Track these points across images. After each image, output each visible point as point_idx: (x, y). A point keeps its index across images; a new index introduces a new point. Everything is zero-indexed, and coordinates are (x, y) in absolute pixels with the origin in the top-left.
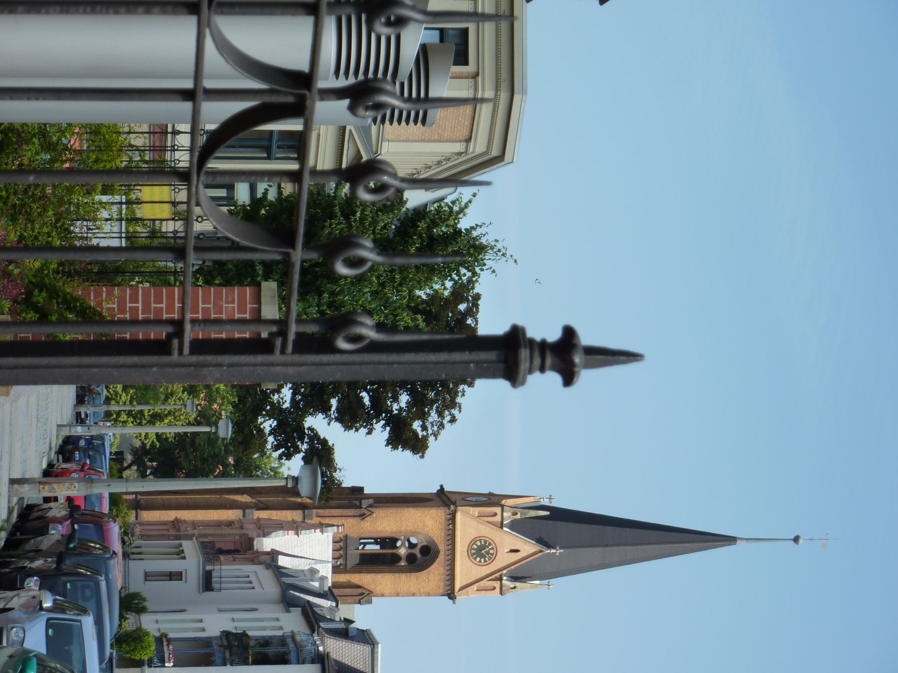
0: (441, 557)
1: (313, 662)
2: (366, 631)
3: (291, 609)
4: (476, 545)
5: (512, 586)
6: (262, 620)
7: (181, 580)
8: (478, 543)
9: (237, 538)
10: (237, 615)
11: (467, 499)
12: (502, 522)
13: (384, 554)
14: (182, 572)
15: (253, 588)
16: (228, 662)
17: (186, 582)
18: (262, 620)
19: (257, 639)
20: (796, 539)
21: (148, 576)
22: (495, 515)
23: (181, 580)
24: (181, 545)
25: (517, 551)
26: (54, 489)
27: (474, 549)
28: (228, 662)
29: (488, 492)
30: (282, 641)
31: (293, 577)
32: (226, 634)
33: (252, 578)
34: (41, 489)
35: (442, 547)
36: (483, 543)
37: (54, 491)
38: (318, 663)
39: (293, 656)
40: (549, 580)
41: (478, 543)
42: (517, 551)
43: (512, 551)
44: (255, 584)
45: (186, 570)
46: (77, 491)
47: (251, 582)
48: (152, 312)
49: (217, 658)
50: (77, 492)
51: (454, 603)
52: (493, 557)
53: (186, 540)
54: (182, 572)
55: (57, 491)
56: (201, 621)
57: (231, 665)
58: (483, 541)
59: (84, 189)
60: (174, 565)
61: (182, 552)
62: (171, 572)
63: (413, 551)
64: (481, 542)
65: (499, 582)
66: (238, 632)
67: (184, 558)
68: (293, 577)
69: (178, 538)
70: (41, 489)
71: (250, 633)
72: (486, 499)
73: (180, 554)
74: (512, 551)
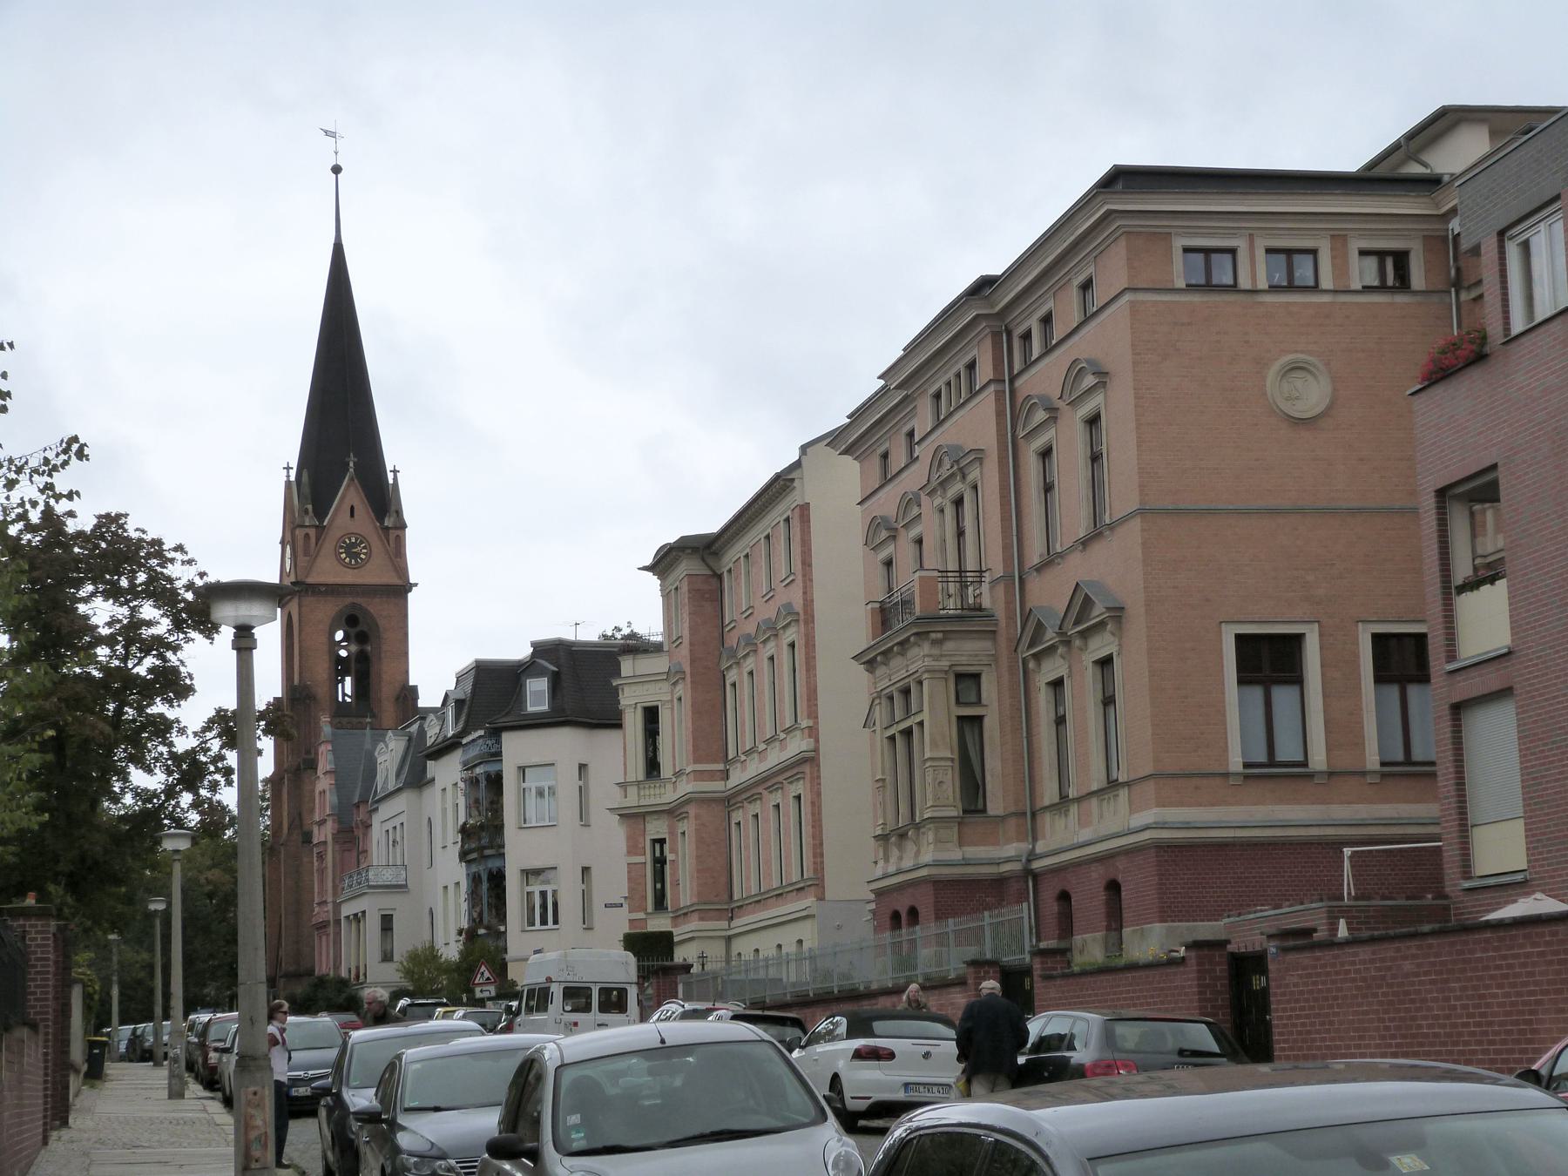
0: (359, 600)
1: (499, 742)
2: (457, 678)
3: (429, 776)
4: (345, 558)
5: (395, 515)
6: (444, 810)
7: (392, 915)
8: (343, 556)
9: (337, 847)
10: (438, 843)
11: (288, 570)
12: (317, 527)
13: (357, 672)
14: (382, 916)
15: (402, 824)
16: (502, 851)
17: (1494, 467)
18: (444, 810)
19: (469, 815)
20: (337, 170)
21: (387, 957)
22: (307, 536)
23: (392, 915)
24: (347, 917)
25: (352, 508)
26: (258, 1139)
27: (351, 561)
28: (502, 851)
29: (280, 546)
30: (473, 782)
31: (387, 776)
32: (463, 856)
33: (389, 826)
34: (258, 1165)
35: (349, 600)
36: (343, 550)
37: (263, 1137)
38: (500, 736)
39: (492, 768)
40: (388, 472)
41: (343, 556)
42: (352, 508)
43: (352, 515)
44: (397, 822)
45: (380, 909)
46: (263, 1087)
47: (395, 828)
48: (1347, 863)
49: (493, 864)
50: (266, 1088)
51: (416, 585)
52: (362, 539)
53: (340, 912)
54: (382, 916)
55: (263, 1131)
56: (446, 887)
57: (504, 847)
58: (341, 551)
59: (50, 1010)
60: (373, 925)
61: (356, 915)
62: (382, 929)
63: (353, 635)
64: (342, 553)
65: (391, 531)
66: (459, 840)
67: (364, 912)
68: (387, 776)
69: (338, 922)
70: (258, 1165)
71: (462, 820)
72: (288, 546)
73: (358, 918)
74: (352, 515)
